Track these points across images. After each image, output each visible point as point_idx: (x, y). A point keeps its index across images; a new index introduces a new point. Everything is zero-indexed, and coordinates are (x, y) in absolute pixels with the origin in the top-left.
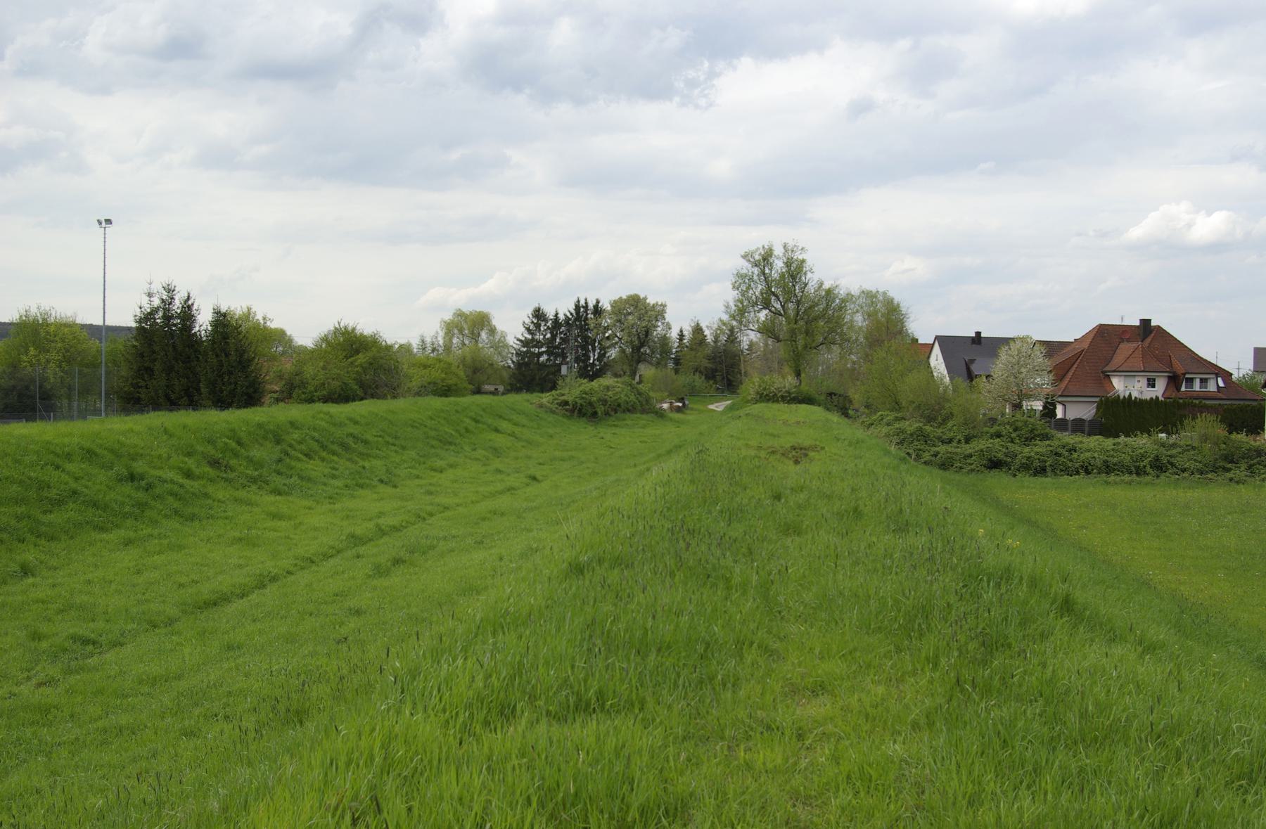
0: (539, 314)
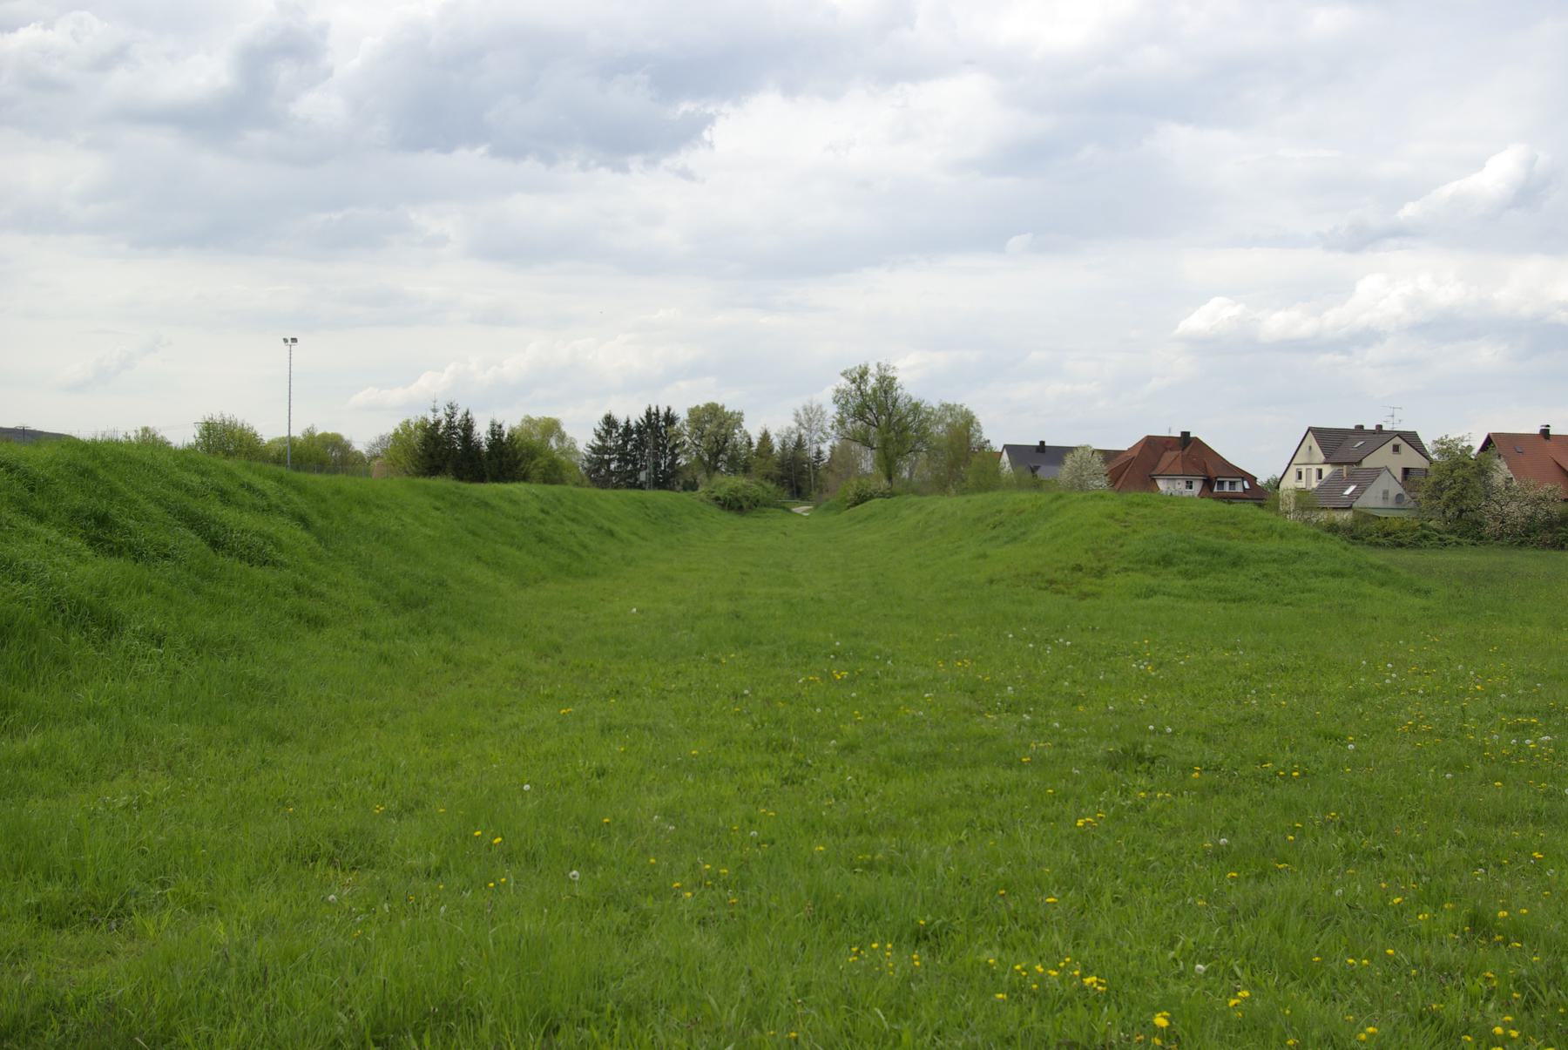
0: (610, 422)
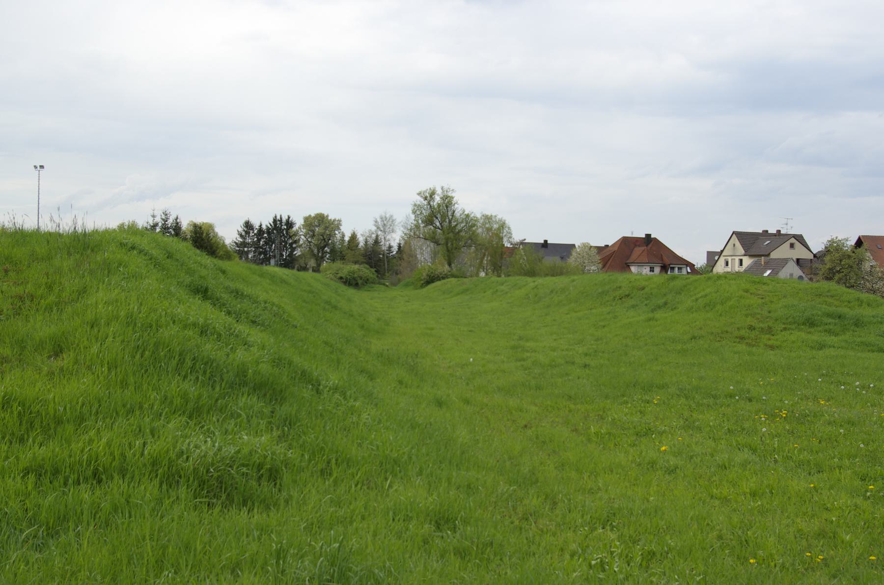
0: (248, 225)
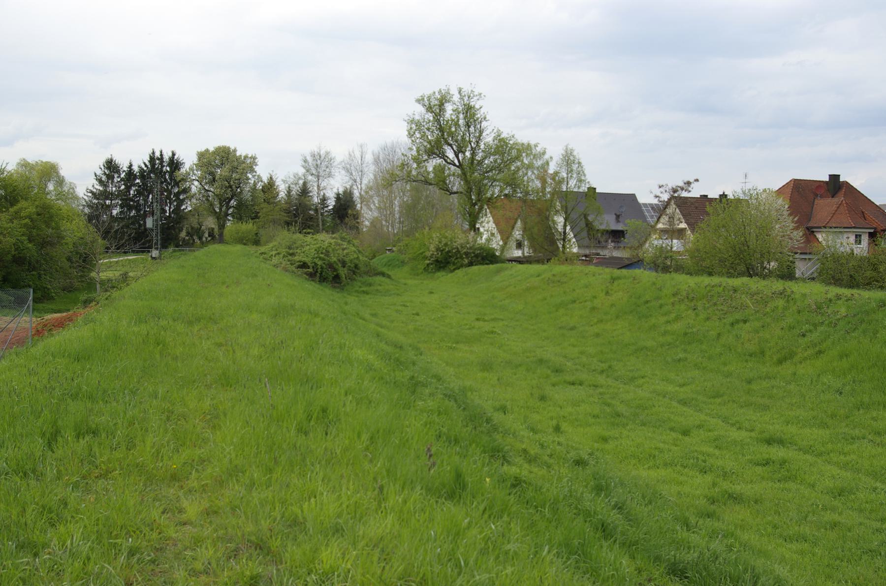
0: (111, 166)
